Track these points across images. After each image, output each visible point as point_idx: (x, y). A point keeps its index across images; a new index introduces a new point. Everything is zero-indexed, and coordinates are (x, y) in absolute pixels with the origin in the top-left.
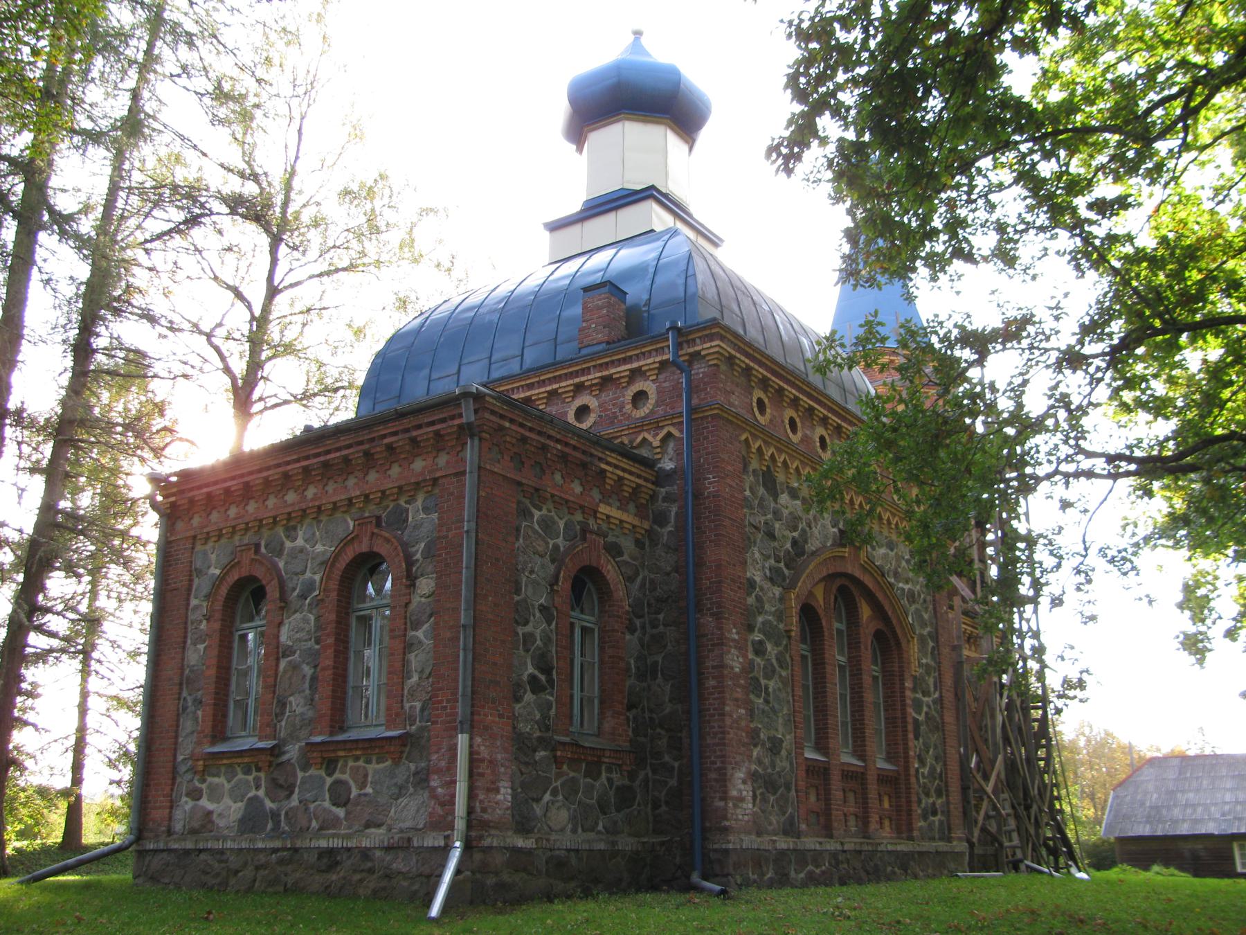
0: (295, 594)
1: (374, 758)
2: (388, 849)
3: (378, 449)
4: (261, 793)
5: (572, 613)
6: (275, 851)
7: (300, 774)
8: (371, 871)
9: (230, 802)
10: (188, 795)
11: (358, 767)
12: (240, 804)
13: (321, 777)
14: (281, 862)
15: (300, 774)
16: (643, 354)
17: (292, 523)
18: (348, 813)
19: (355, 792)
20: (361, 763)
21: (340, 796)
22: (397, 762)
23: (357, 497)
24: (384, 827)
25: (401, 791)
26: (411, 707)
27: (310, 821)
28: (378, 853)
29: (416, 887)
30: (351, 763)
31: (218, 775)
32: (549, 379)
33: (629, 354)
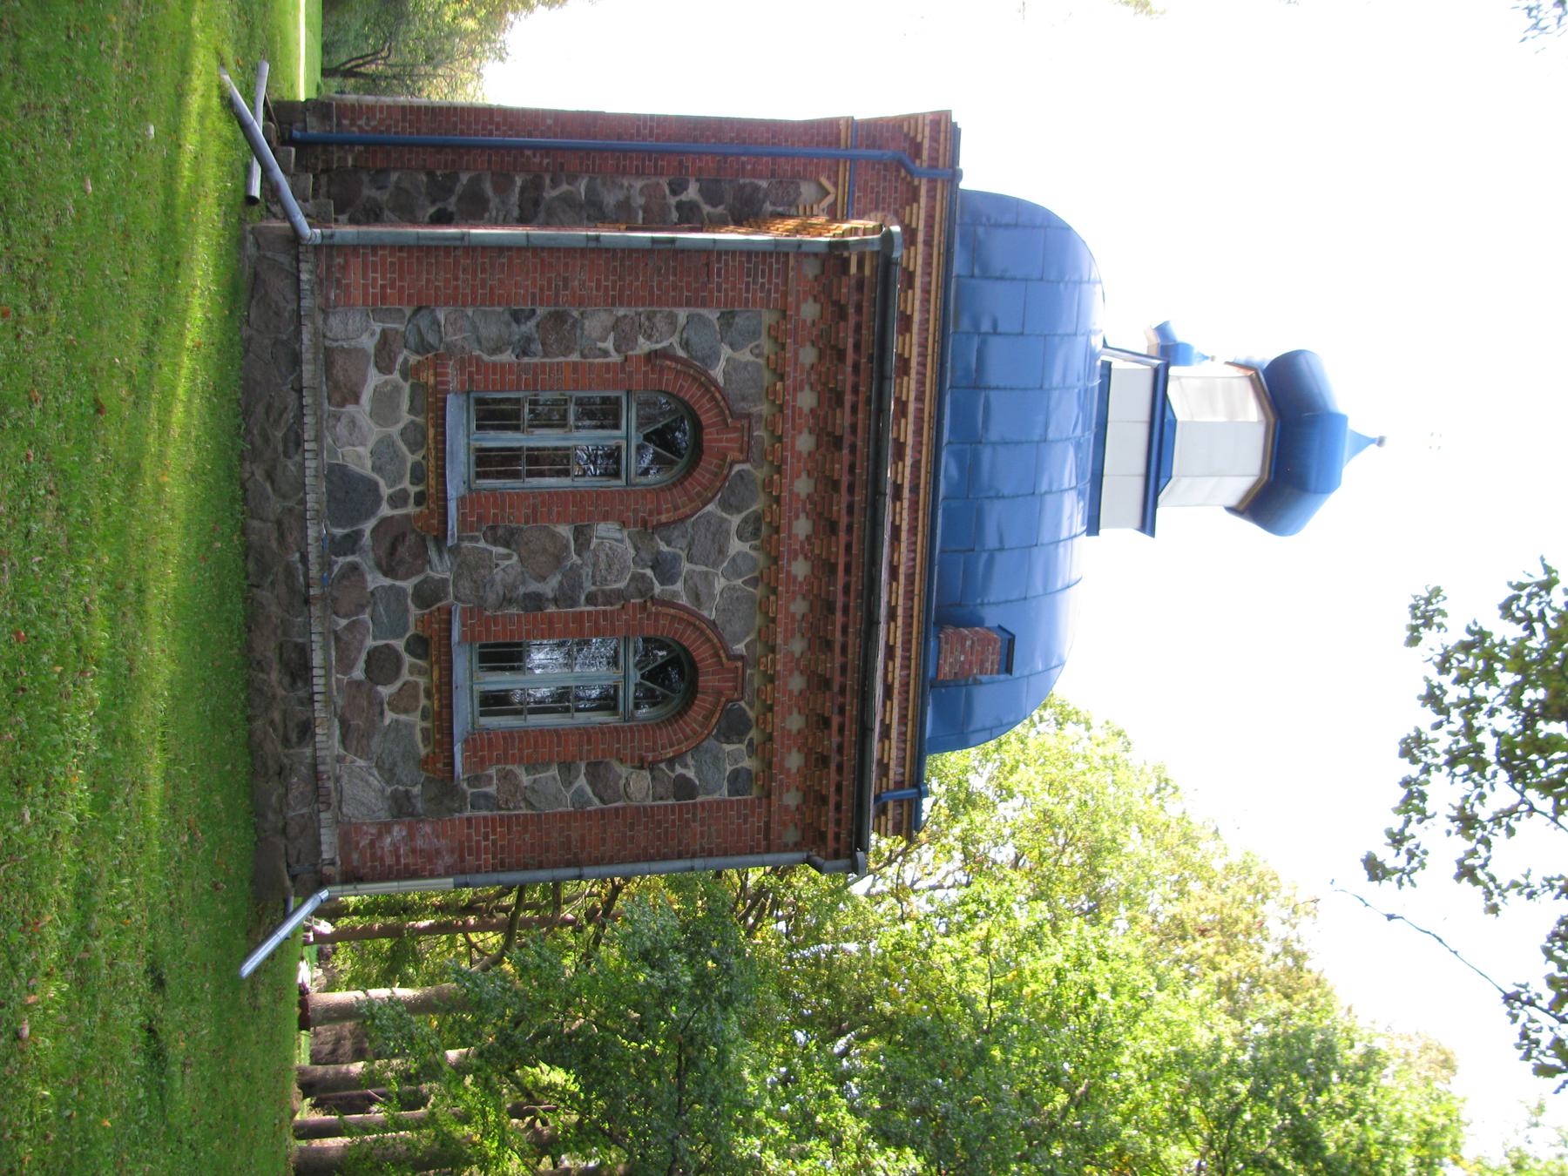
0: (664, 548)
4: (385, 510)
6: (304, 558)
7: (408, 585)
8: (286, 741)
9: (371, 442)
10: (384, 332)
11: (416, 698)
12: (369, 464)
13: (405, 630)
14: (289, 571)
15: (408, 585)
16: (905, 742)
17: (764, 530)
18: (359, 684)
19: (385, 691)
20: (423, 702)
21: (382, 664)
22: (424, 763)
23: (774, 662)
24: (342, 751)
25: (390, 775)
26: (491, 778)
27: (346, 616)
28: (308, 751)
29: (271, 816)
30: (422, 681)
31: (412, 410)
32: (912, 608)
33: (910, 724)
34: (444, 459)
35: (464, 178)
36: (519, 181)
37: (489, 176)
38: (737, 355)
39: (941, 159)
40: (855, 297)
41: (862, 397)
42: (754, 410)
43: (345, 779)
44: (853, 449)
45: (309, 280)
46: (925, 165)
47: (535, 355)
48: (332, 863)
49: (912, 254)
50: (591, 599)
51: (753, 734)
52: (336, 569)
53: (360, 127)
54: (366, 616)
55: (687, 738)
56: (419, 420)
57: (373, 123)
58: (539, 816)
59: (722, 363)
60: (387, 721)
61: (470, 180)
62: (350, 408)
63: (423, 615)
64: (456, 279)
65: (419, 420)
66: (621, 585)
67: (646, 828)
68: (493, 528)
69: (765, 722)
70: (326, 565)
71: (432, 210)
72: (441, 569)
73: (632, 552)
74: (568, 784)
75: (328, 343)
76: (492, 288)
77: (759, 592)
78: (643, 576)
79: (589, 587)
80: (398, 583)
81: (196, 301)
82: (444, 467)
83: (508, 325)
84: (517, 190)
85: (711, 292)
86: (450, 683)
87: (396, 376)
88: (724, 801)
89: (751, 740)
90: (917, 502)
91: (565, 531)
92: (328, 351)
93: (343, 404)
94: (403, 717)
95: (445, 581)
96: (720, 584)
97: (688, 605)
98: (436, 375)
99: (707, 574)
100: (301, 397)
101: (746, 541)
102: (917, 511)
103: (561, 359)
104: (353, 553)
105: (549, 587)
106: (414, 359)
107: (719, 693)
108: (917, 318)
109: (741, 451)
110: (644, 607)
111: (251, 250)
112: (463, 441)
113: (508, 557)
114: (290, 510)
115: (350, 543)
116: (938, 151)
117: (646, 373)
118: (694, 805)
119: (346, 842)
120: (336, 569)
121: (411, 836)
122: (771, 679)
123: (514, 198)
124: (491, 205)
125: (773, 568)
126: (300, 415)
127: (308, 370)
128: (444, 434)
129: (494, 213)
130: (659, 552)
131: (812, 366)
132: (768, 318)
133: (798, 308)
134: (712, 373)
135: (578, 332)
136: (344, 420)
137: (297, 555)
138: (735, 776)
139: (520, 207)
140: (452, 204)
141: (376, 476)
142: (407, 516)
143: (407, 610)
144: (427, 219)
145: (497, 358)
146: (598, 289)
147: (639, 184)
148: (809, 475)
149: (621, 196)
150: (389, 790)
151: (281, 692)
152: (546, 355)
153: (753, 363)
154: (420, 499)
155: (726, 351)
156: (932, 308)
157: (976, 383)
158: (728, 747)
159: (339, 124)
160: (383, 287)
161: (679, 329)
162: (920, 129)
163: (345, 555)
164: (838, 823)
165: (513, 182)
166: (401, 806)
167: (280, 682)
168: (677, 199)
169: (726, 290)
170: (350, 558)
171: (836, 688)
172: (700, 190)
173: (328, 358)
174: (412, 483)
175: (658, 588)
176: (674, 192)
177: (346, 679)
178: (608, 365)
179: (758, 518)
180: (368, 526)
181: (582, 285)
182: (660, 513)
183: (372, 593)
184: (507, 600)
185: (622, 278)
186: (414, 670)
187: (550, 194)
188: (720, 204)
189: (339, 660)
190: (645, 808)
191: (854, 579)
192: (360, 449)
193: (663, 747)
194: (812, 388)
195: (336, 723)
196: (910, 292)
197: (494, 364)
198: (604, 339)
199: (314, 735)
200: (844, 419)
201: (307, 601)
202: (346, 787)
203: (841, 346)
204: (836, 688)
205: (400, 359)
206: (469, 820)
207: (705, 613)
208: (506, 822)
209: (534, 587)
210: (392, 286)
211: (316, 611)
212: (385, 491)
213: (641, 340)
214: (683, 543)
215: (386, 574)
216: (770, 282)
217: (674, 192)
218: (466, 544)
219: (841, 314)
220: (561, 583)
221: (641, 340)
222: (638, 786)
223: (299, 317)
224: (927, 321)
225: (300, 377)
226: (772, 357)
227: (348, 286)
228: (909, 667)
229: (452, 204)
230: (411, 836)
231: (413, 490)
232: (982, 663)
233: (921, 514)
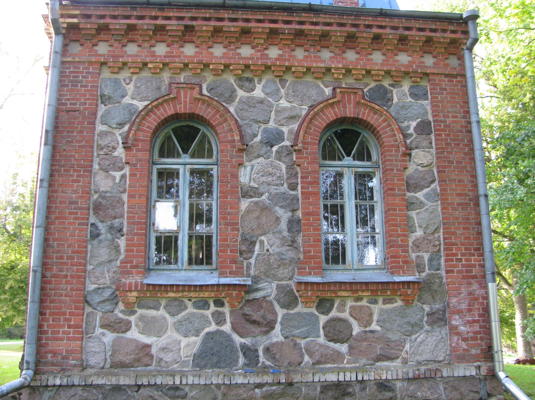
4: (227, 328)
6: (259, 386)
7: (281, 312)
9: (178, 336)
10: (102, 326)
12: (193, 339)
15: (281, 312)
18: (351, 348)
19: (356, 329)
20: (364, 303)
23: (337, 69)
24: (399, 360)
28: (399, 384)
30: (350, 303)
31: (157, 308)
41: (159, 14)
42: (167, 82)
44: (193, 19)
48: (479, 367)
50: (294, 187)
51: (386, 83)
56: (163, 303)
58: (444, 224)
59: (135, 102)
60: (378, 328)
62: (154, 351)
64: (66, 276)
65: (163, 303)
66: (283, 167)
69: (378, 75)
70: (265, 370)
73: (260, 159)
75: (108, 366)
76: (73, 252)
82: (195, 286)
83: (100, 241)
87: (132, 318)
91: (244, 204)
94: (375, 317)
96: (284, 103)
98: (130, 291)
104: (257, 351)
105: (284, 215)
106: (121, 306)
110: (299, 151)
113: (262, 242)
120: (268, 363)
121: (459, 312)
127: (124, 381)
130: (261, 142)
135: (108, 195)
136: (162, 355)
137: (257, 390)
141: (202, 334)
142: (231, 312)
143: (298, 314)
146: (78, 181)
150: (427, 327)
152: (122, 216)
154: (219, 303)
155: (127, 100)
158: (395, 100)
163: (258, 356)
169: (85, 100)
174: (208, 308)
175: (287, 143)
179: (240, 79)
180: (238, 340)
181: (75, 192)
182: (234, 141)
183: (286, 338)
185: (72, 166)
186: (341, 309)
189: (334, 361)
190: (437, 153)
192: (183, 345)
197: (127, 251)
198: (114, 178)
202: (425, 357)
205: (121, 315)
206: (447, 272)
207: (304, 112)
208: (449, 246)
209: (284, 225)
210: (69, 320)
211: (297, 378)
212: (213, 327)
213: (116, 154)
215: (273, 328)
216: (82, 72)
220: (281, 207)
221: (116, 154)
226: (132, 70)
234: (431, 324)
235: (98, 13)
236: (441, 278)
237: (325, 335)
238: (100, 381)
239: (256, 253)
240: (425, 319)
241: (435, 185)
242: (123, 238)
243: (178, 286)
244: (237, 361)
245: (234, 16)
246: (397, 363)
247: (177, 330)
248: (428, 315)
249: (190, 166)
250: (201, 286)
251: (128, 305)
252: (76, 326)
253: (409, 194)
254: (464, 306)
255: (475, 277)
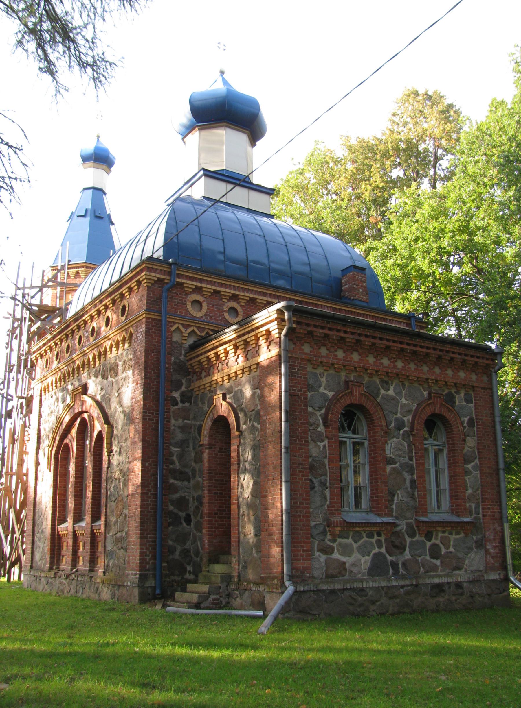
1: (454, 532)
2: (470, 582)
3: (446, 358)
4: (383, 550)
5: (340, 434)
6: (402, 587)
7: (408, 540)
8: (462, 594)
9: (360, 556)
10: (319, 551)
11: (446, 537)
12: (367, 558)
14: (407, 593)
15: (408, 540)
17: (386, 379)
18: (442, 562)
19: (443, 551)
20: (446, 534)
21: (435, 553)
23: (431, 380)
24: (463, 570)
25: (470, 549)
28: (465, 585)
30: (440, 534)
31: (347, 538)
34: (368, 523)
35: (171, 508)
36: (172, 481)
37: (170, 495)
38: (324, 385)
39: (165, 269)
40: (304, 327)
41: (342, 328)
42: (343, 379)
43: (471, 568)
44: (360, 335)
45: (304, 586)
46: (168, 278)
47: (326, 480)
48: (499, 574)
49: (206, 290)
50: (411, 459)
51: (453, 391)
52: (404, 572)
53: (150, 560)
54: (420, 559)
55: (456, 420)
56: (351, 534)
57: (148, 553)
58: (482, 486)
59: (326, 392)
60: (453, 550)
61: (172, 505)
62: (347, 566)
63: (419, 533)
64: (300, 516)
65: (351, 534)
66: (406, 445)
67: (484, 440)
68: (389, 501)
69: (450, 386)
70: (403, 577)
71: (185, 524)
72: (402, 526)
73: (395, 439)
74: (471, 473)
75: (324, 577)
76: (303, 499)
77: (407, 384)
78: (403, 434)
79: (407, 459)
80: (408, 545)
81: (470, 643)
82: (371, 523)
83: (316, 492)
84: (176, 482)
85: (302, 394)
86: (443, 522)
87: (335, 545)
88: (475, 406)
89: (455, 392)
90: (306, 302)
91: (389, 468)
92: (327, 576)
93: (345, 569)
94: (452, 543)
95: (407, 524)
96: (404, 401)
97: (412, 415)
98: (337, 526)
99: (401, 406)
100: (347, 589)
101: (390, 387)
102: (309, 303)
103: (327, 467)
104: (398, 565)
105: (407, 477)
106: (329, 537)
107: (441, 405)
108: (233, 292)
109: (360, 386)
110: (414, 435)
111: (291, 614)
112: (352, 514)
113: (398, 495)
114: (386, 593)
115: (394, 565)
116: (161, 270)
117: (332, 428)
118: (477, 419)
119: (493, 569)
120: (404, 572)
121: (490, 541)
122: (437, 381)
123: (178, 483)
124: (183, 495)
125: (400, 376)
126: (353, 589)
127: (338, 586)
128: (359, 523)
129: (186, 494)
130: (395, 427)
131: (328, 350)
132: (310, 369)
133: (306, 354)
134: (330, 397)
135: (317, 459)
136: (352, 569)
137: (401, 590)
138: (466, 400)
139: (183, 481)
140: (182, 514)
141: (371, 555)
142: (385, 540)
143: (417, 541)
144: (189, 527)
145: (328, 498)
146: (302, 449)
147: (173, 421)
148: (367, 356)
149: (178, 431)
150: (475, 550)
151: (447, 597)
152: (326, 475)
153: (327, 378)
154: (379, 534)
155: (322, 390)
156: (229, 283)
157: (246, 265)
158: (457, 403)
159: (148, 570)
160: (304, 551)
161: (314, 411)
162: (152, 278)
163: (399, 568)
164: (483, 358)
165: (172, 484)
166: (480, 545)
167: (443, 597)
168: (179, 402)
169: (301, 387)
170: (400, 566)
171: (441, 353)
172: (176, 391)
173: (330, 577)
174: (373, 538)
175: (406, 429)
176: (177, 404)
177: (440, 568)
178: (329, 446)
179: (382, 381)
180: (389, 558)
181: (301, 456)
182: (382, 426)
183: (412, 556)
184: (412, 496)
185: (298, 437)
186: (436, 539)
187: (177, 466)
188: (181, 381)
189: (434, 571)
190: (478, 440)
191: (406, 341)
192: (362, 562)
193: (459, 431)
194: (336, 351)
195: (454, 572)
196: (222, 293)
197: (331, 499)
198: (319, 447)
199: (461, 582)
200: (350, 338)
201: (416, 585)
202: (475, 568)
203: (323, 335)
204: (441, 353)
205: (329, 543)
206: (484, 516)
207: (414, 408)
208: (484, 499)
209: (408, 484)
210: (303, 547)
211: (421, 581)
212: (376, 550)
213: (319, 429)
214: (391, 415)
215: (405, 550)
216: (297, 366)
217: (177, 404)
218: (394, 514)
219: (310, 333)
220: (407, 472)
221: (319, 429)
222: (471, 442)
223: (318, 590)
224: (234, 286)
225: (339, 590)
226: (325, 368)
227: (303, 568)
228: (367, 315)
229: (182, 514)
230: (490, 541)
231: (376, 537)
232: (362, 281)
233: (311, 301)
234: (477, 547)
235: (307, 322)
236: (480, 519)
237: (430, 555)
238: (325, 587)
239: (395, 501)
240: (474, 544)
241: (477, 461)
242: (327, 490)
243: (362, 523)
244: (389, 571)
245: (381, 336)
246: (462, 572)
247: (359, 552)
248: (476, 542)
249: (352, 440)
250: (373, 523)
251: (333, 535)
252: (307, 551)
253: (465, 466)
254: (492, 537)
255: (496, 519)
